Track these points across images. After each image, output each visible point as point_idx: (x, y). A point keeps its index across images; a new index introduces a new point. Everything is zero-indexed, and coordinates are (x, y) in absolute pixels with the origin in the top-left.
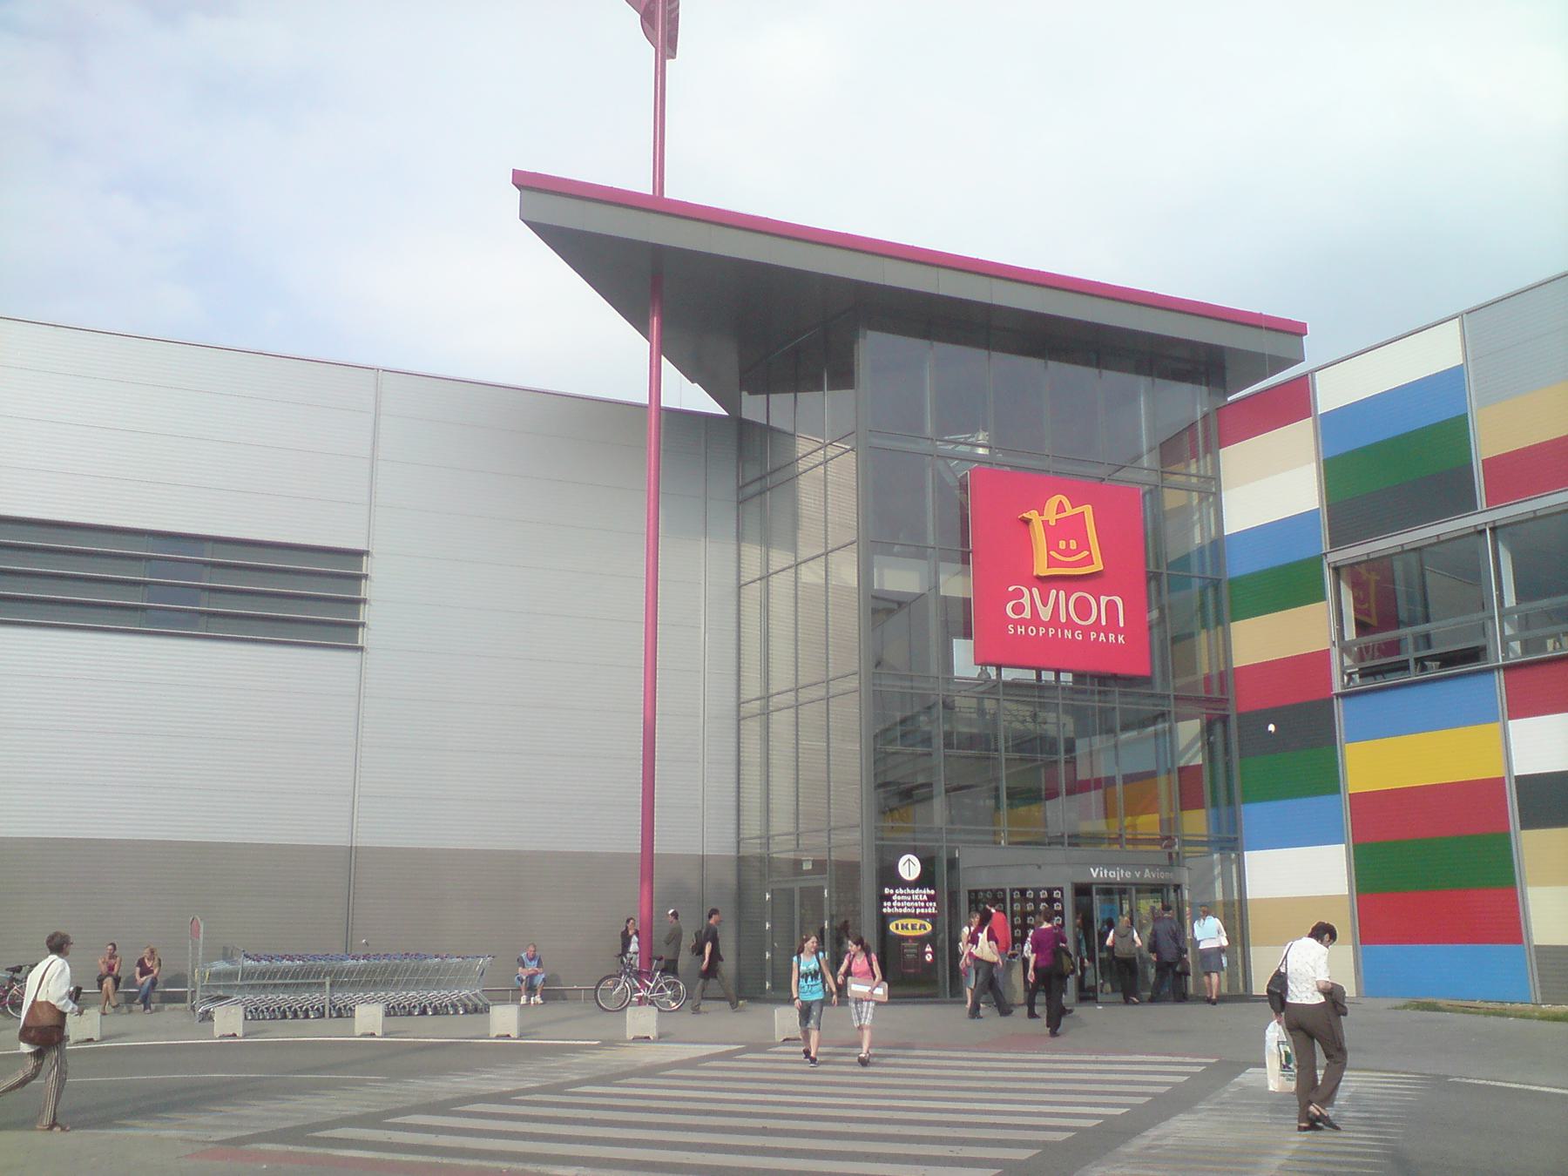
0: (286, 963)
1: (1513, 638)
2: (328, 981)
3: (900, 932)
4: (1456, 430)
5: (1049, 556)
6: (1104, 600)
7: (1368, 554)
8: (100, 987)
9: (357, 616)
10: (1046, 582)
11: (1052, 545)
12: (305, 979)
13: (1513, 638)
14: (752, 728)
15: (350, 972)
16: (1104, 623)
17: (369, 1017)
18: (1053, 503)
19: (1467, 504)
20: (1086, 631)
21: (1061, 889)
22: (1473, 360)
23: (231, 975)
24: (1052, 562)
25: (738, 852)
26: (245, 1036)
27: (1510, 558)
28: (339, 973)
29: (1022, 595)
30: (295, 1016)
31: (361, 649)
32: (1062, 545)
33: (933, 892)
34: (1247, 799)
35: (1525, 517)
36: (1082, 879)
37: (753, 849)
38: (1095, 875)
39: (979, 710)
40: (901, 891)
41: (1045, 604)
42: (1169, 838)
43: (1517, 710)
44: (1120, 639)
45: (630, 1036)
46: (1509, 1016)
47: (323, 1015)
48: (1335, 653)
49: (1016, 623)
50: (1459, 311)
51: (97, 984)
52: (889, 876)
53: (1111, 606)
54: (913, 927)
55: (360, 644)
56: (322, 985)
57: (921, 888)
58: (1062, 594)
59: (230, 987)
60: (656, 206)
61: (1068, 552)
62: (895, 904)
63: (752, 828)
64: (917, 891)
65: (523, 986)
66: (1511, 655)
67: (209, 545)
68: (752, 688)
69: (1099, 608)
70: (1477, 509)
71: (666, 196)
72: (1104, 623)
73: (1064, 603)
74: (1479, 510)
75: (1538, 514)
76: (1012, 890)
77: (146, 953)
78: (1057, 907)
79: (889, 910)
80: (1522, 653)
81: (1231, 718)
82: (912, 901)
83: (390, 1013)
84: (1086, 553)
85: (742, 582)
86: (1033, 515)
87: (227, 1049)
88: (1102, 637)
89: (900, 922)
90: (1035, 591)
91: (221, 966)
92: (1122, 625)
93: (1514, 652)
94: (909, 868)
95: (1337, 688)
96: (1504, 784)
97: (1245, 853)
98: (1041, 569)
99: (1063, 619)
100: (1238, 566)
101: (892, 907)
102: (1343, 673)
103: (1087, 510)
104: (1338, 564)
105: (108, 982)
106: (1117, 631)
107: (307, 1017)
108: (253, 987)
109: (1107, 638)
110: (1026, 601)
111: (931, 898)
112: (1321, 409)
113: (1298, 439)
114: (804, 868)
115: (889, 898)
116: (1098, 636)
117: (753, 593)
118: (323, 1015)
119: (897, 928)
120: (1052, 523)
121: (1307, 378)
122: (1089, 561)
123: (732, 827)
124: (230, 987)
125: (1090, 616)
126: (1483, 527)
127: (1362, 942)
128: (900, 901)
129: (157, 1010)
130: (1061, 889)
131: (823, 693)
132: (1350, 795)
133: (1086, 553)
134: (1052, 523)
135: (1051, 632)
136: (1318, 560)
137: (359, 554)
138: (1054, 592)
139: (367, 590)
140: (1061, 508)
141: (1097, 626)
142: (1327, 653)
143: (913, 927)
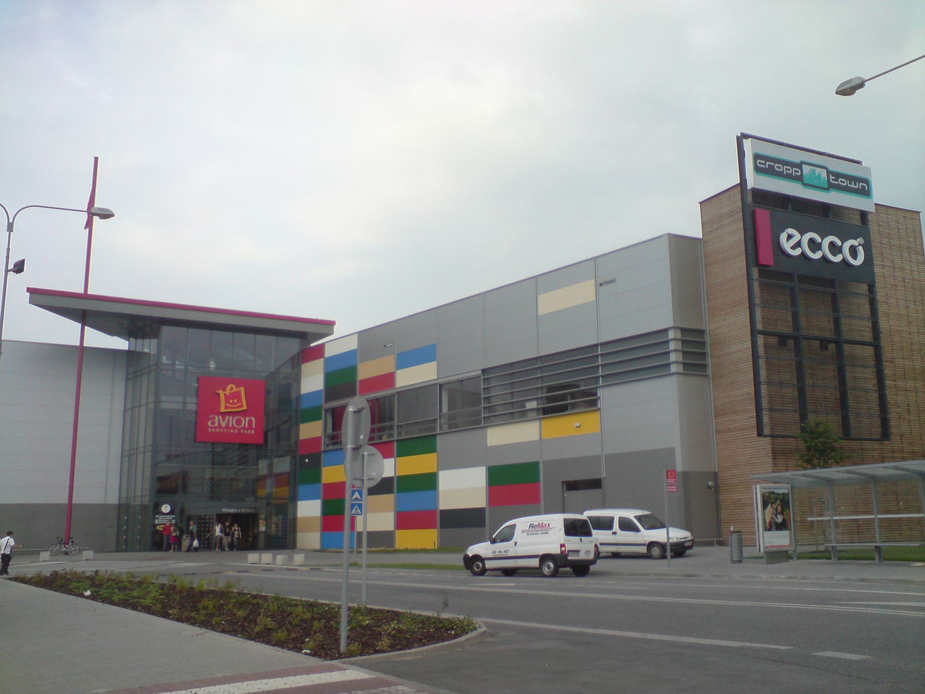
4: (353, 370)
5: (226, 405)
6: (247, 419)
10: (224, 414)
14: (126, 459)
16: (247, 426)
18: (229, 387)
20: (239, 429)
24: (226, 407)
29: (215, 418)
32: (231, 401)
36: (219, 512)
37: (124, 501)
40: (162, 516)
41: (224, 421)
44: (253, 432)
48: (323, 438)
49: (211, 428)
53: (250, 422)
58: (231, 418)
60: (85, 296)
61: (233, 403)
63: (124, 495)
69: (245, 422)
72: (247, 426)
73: (232, 421)
86: (221, 392)
90: (220, 417)
92: (254, 426)
94: (166, 508)
95: (323, 449)
98: (222, 410)
99: (231, 426)
100: (304, 405)
103: (242, 389)
104: (441, 384)
110: (216, 420)
113: (318, 365)
115: (158, 518)
119: (160, 528)
120: (228, 394)
122: (241, 406)
125: (831, 253)
130: (213, 515)
134: (228, 394)
135: (226, 430)
136: (322, 405)
140: (232, 389)
141: (244, 428)
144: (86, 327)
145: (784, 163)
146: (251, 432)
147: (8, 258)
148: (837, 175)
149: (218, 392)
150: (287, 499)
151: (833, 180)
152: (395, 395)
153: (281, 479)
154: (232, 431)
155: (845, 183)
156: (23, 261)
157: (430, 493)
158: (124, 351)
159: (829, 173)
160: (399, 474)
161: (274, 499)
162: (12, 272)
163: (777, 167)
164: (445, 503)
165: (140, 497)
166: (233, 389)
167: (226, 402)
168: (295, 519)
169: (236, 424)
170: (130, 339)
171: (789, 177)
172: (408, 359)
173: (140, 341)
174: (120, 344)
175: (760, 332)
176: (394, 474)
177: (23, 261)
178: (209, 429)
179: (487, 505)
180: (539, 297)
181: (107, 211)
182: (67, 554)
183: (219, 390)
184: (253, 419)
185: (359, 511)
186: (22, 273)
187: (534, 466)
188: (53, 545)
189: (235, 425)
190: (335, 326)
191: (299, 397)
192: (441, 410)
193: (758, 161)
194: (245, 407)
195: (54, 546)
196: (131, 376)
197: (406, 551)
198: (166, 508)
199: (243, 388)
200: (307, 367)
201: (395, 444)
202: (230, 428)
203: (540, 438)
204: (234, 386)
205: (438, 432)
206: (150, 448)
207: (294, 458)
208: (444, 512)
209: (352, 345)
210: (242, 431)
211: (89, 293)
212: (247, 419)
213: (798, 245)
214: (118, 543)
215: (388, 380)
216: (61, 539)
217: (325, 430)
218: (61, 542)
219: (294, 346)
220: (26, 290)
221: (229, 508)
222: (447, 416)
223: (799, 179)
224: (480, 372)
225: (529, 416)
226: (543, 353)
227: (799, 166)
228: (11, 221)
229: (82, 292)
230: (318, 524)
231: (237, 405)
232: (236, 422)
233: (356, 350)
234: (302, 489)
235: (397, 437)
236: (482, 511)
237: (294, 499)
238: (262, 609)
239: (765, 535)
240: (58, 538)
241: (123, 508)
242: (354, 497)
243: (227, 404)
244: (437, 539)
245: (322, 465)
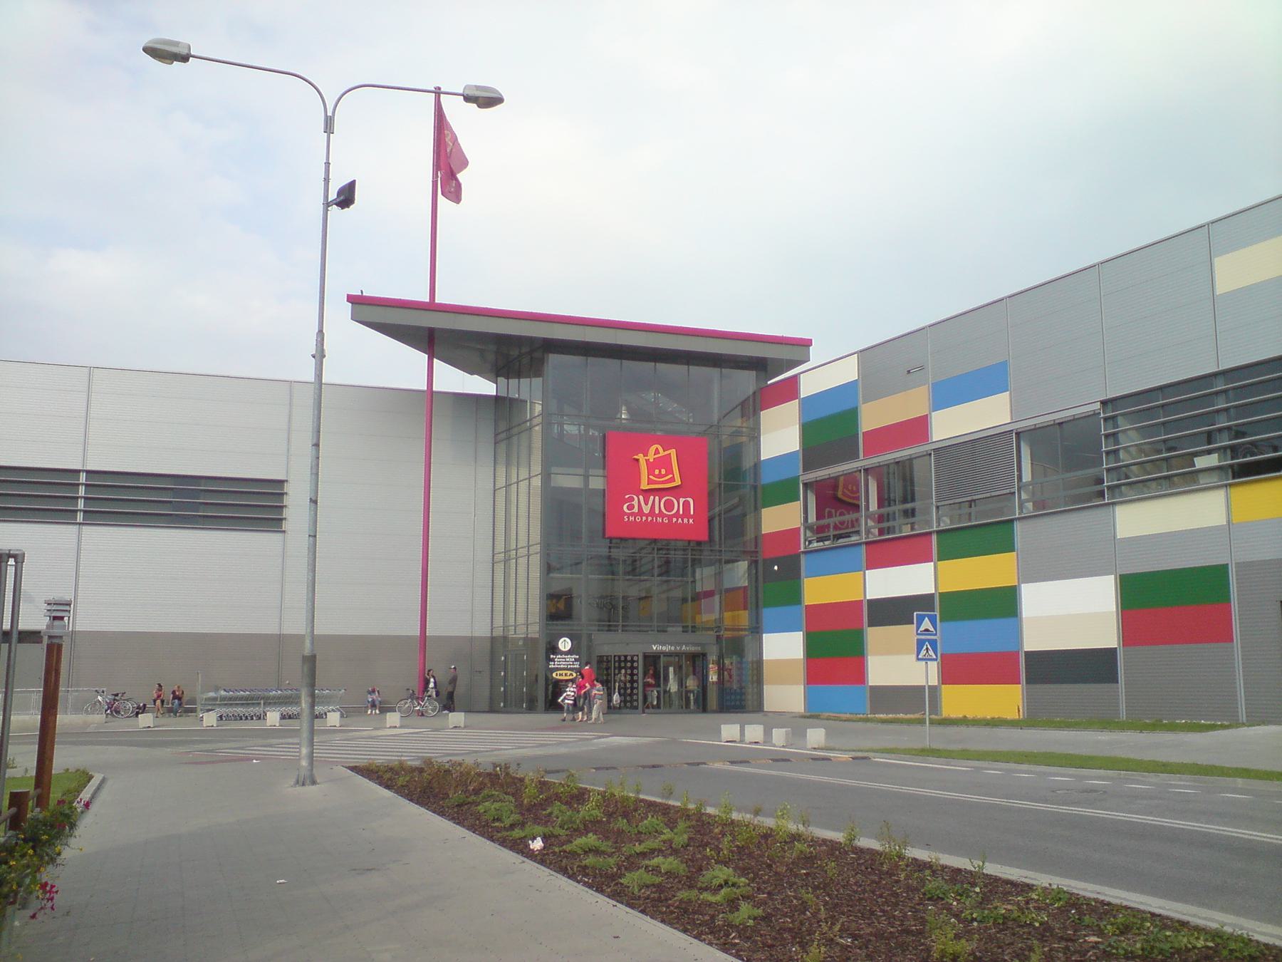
0: (861, 716)
1: (1027, 501)
2: (262, 702)
3: (559, 677)
4: (851, 416)
6: (682, 500)
7: (1035, 425)
8: (155, 704)
9: (282, 515)
10: (647, 493)
11: (650, 472)
12: (248, 701)
13: (1027, 501)
14: (500, 568)
15: (274, 697)
16: (681, 512)
17: (273, 717)
18: (653, 449)
19: (854, 455)
20: (670, 518)
21: (637, 656)
22: (1104, 296)
23: (215, 699)
24: (650, 482)
25: (492, 634)
26: (217, 726)
27: (876, 484)
28: (268, 698)
29: (633, 500)
30: (247, 718)
32: (657, 472)
33: (578, 657)
34: (765, 606)
35: (1069, 419)
37: (499, 632)
38: (655, 648)
40: (560, 656)
41: (646, 504)
42: (719, 627)
43: (871, 566)
44: (691, 521)
45: (388, 726)
47: (260, 718)
49: (628, 515)
50: (1206, 221)
51: (153, 703)
52: (553, 649)
53: (686, 504)
54: (566, 675)
55: (283, 529)
56: (259, 704)
57: (572, 655)
58: (657, 498)
59: (214, 705)
60: (431, 307)
61: (660, 476)
62: (556, 663)
63: (499, 622)
64: (569, 656)
65: (369, 705)
66: (942, 525)
67: (203, 481)
68: (500, 547)
69: (678, 505)
70: (928, 441)
71: (437, 301)
72: (681, 512)
73: (659, 503)
74: (930, 441)
75: (1076, 417)
76: (615, 656)
77: (176, 688)
78: (635, 664)
79: (553, 666)
80: (1033, 509)
81: (759, 562)
82: (565, 661)
83: (283, 717)
84: (671, 476)
85: (496, 488)
86: (640, 457)
87: (209, 731)
88: (680, 520)
89: (558, 672)
90: (641, 497)
91: (212, 694)
92: (692, 513)
93: (1027, 508)
96: (1228, 568)
97: (764, 635)
98: (644, 486)
99: (657, 512)
100: (767, 478)
101: (554, 665)
102: (805, 540)
103: (673, 452)
104: (1019, 430)
105: (158, 702)
106: (689, 517)
107: (252, 719)
108: (226, 704)
109: (683, 521)
110: (635, 503)
111: (576, 660)
112: (802, 397)
113: (792, 408)
115: (553, 660)
116: (677, 520)
117: (501, 495)
118: (260, 718)
119: (557, 675)
120: (651, 460)
123: (489, 621)
124: (214, 705)
126: (859, 468)
127: (807, 684)
128: (558, 661)
129: (180, 716)
130: (637, 656)
132: (939, 593)
133: (671, 476)
134: (651, 460)
135: (650, 519)
137: (281, 482)
138: (652, 498)
139: (287, 501)
140: (657, 452)
142: (799, 528)
143: (566, 675)
144: (435, 360)
146: (688, 521)
147: (327, 180)
149: (636, 457)
150: (745, 630)
152: (930, 454)
153: (734, 598)
154: (659, 520)
156: (354, 181)
157: (1011, 620)
158: (490, 396)
161: (726, 629)
162: (334, 206)
164: (1034, 641)
165: (502, 628)
166: (659, 453)
168: (759, 663)
169: (666, 510)
170: (499, 379)
172: (949, 394)
173: (513, 382)
174: (483, 386)
176: (934, 589)
177: (354, 181)
179: (1119, 644)
180: (1217, 261)
181: (495, 93)
182: (423, 715)
183: (637, 455)
185: (931, 652)
186: (351, 207)
187: (1222, 570)
188: (401, 700)
189: (665, 512)
190: (811, 348)
191: (757, 465)
192: (1020, 477)
194: (678, 482)
195: (403, 702)
196: (503, 436)
197: (964, 721)
198: (565, 644)
199: (674, 450)
200: (767, 416)
201: (934, 537)
202: (657, 516)
203: (1229, 522)
205: (1017, 516)
206: (538, 548)
207: (754, 563)
208: (1032, 656)
209: (848, 372)
211: (437, 301)
214: (491, 699)
215: (919, 427)
216: (413, 691)
217: (806, 519)
218: (412, 696)
219: (746, 382)
220: (346, 299)
221: (663, 644)
222: (876, 516)
224: (1098, 406)
225: (1201, 482)
226: (1226, 365)
228: (330, 114)
229: (427, 300)
230: (801, 672)
231: (666, 478)
233: (853, 384)
234: (768, 614)
235: (866, 538)
236: (1112, 652)
237: (757, 630)
238: (951, 904)
240: (408, 689)
241: (497, 644)
242: (922, 628)
243: (651, 477)
244: (1021, 701)
245: (803, 573)
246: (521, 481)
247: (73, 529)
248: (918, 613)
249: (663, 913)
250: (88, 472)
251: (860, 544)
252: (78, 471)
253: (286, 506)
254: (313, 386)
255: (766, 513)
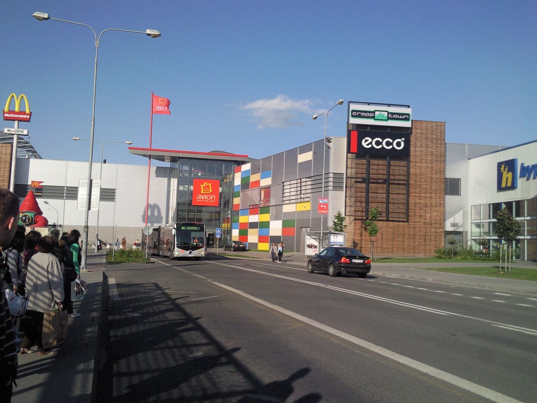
6: (212, 196)
11: (204, 189)
20: (209, 200)
24: (204, 191)
31: (115, 202)
39: (409, 196)
41: (203, 196)
44: (214, 201)
46: (353, 273)
49: (198, 200)
53: (213, 197)
58: (206, 196)
61: (206, 190)
69: (211, 197)
73: (206, 197)
103: (210, 184)
110: (200, 197)
114: (210, 243)
121: (297, 149)
122: (210, 191)
131: (382, 189)
135: (203, 201)
137: (78, 187)
140: (206, 184)
145: (365, 112)
148: (393, 114)
151: (390, 116)
154: (206, 201)
155: (397, 116)
159: (388, 113)
160: (260, 221)
163: (363, 114)
167: (204, 190)
171: (368, 117)
175: (349, 178)
178: (197, 200)
184: (214, 196)
193: (353, 113)
204: (207, 183)
208: (272, 237)
210: (210, 201)
212: (212, 196)
213: (371, 143)
223: (373, 117)
227: (374, 112)
232: (210, 197)
239: (6, 184)
243: (204, 190)
246: (302, 190)
247: (63, 200)
248: (514, 216)
249: (330, 264)
250: (67, 187)
251: (258, 208)
252: (64, 187)
253: (116, 195)
254: (9, 163)
255: (235, 199)
